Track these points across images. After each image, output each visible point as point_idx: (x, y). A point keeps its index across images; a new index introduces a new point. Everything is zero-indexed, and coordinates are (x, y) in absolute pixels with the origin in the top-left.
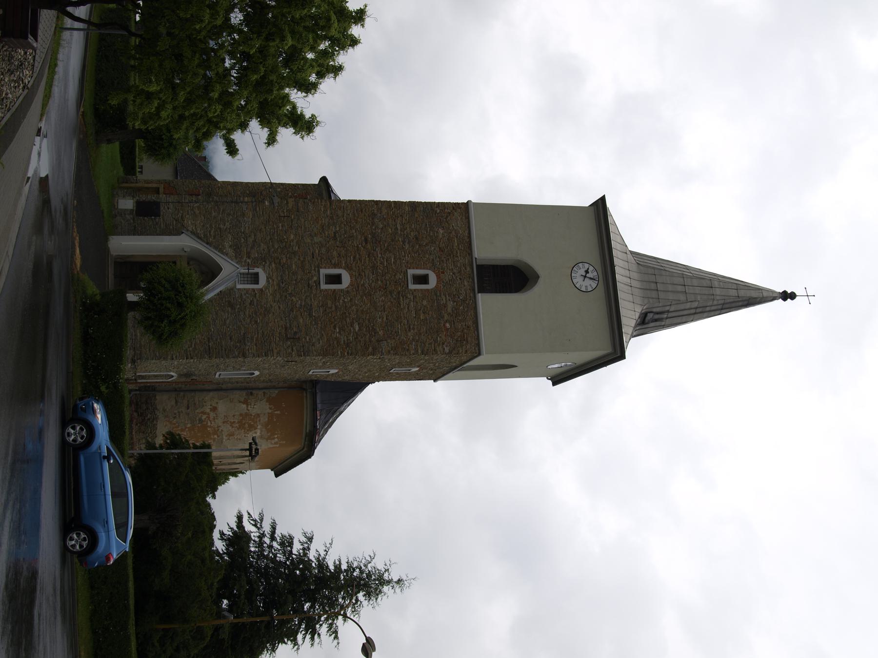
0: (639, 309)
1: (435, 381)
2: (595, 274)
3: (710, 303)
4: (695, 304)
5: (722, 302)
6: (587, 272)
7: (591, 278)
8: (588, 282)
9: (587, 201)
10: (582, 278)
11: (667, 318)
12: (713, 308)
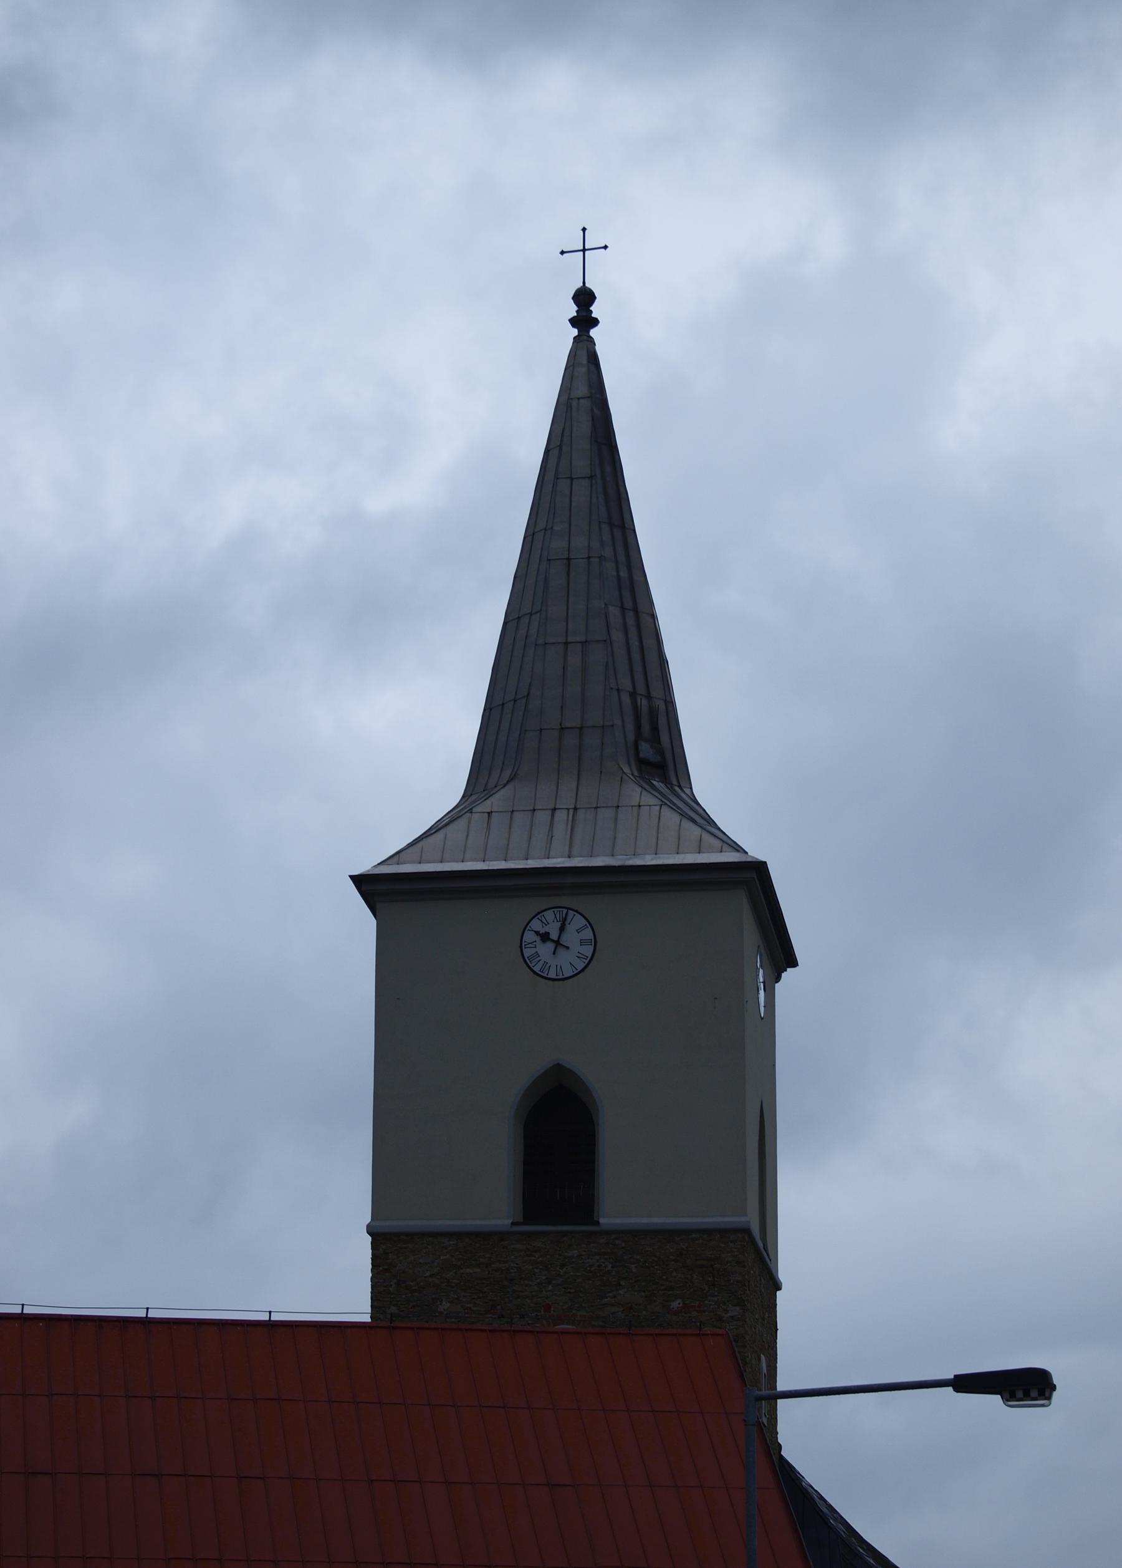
0: (634, 793)
1: (778, 1287)
2: (549, 915)
3: (610, 566)
4: (614, 611)
5: (606, 529)
6: (545, 937)
7: (562, 929)
8: (571, 937)
9: (363, 924)
10: (561, 950)
11: (649, 697)
12: (622, 558)
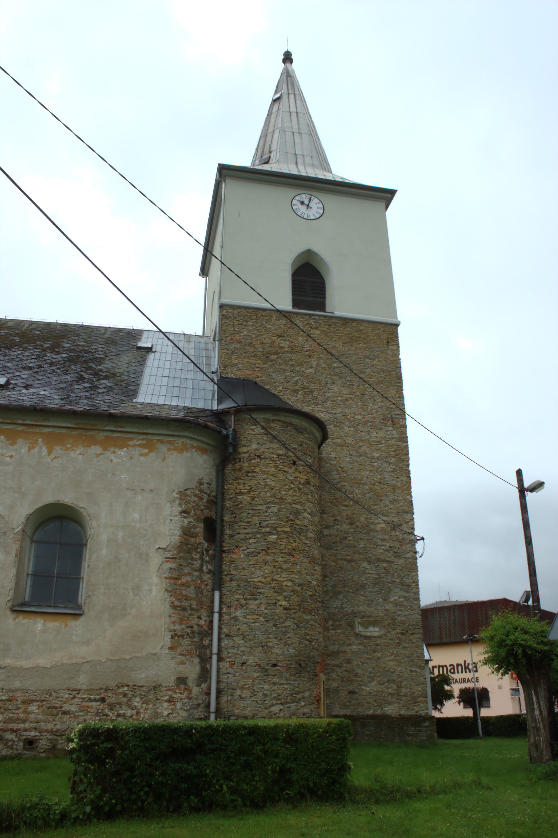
6: (302, 203)
7: (310, 200)
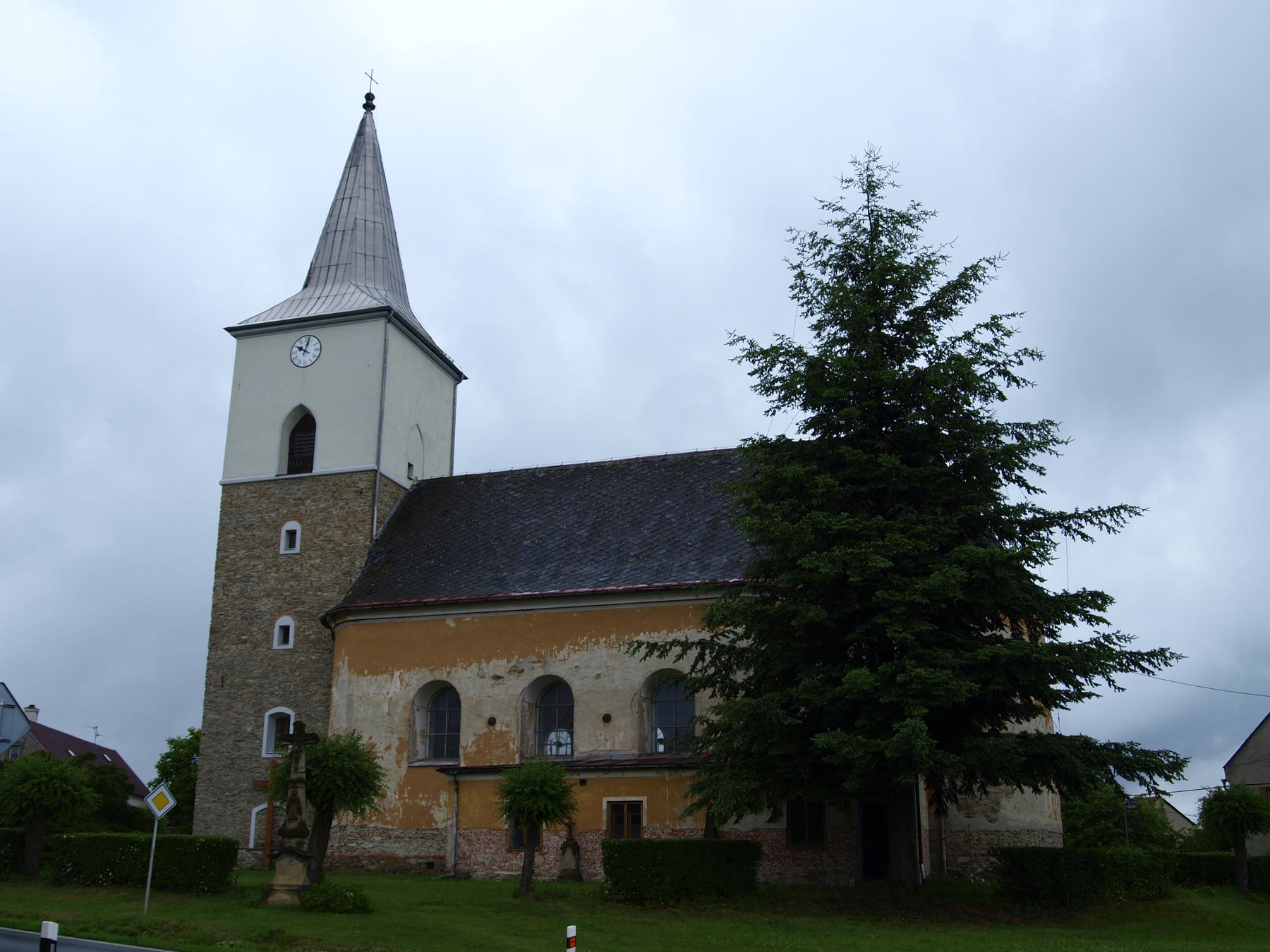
6: (301, 349)
